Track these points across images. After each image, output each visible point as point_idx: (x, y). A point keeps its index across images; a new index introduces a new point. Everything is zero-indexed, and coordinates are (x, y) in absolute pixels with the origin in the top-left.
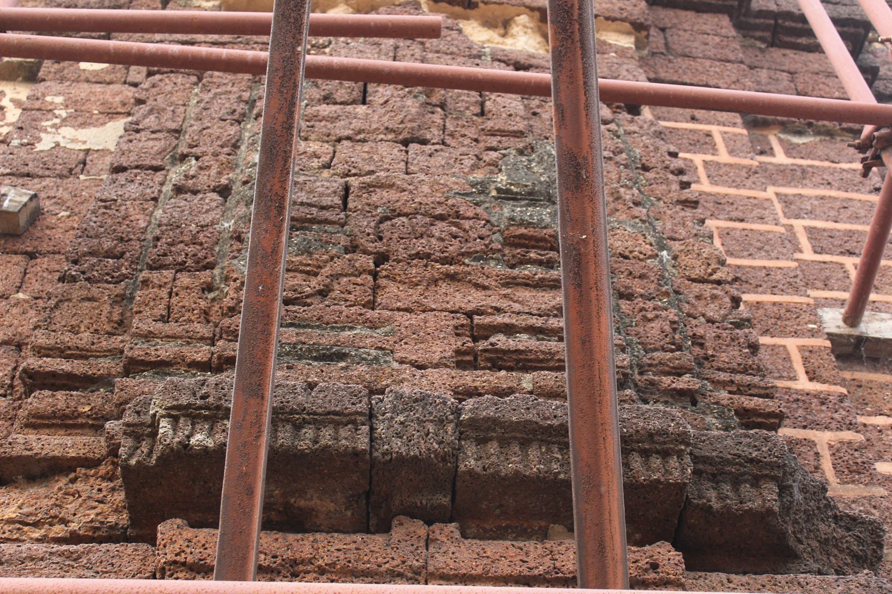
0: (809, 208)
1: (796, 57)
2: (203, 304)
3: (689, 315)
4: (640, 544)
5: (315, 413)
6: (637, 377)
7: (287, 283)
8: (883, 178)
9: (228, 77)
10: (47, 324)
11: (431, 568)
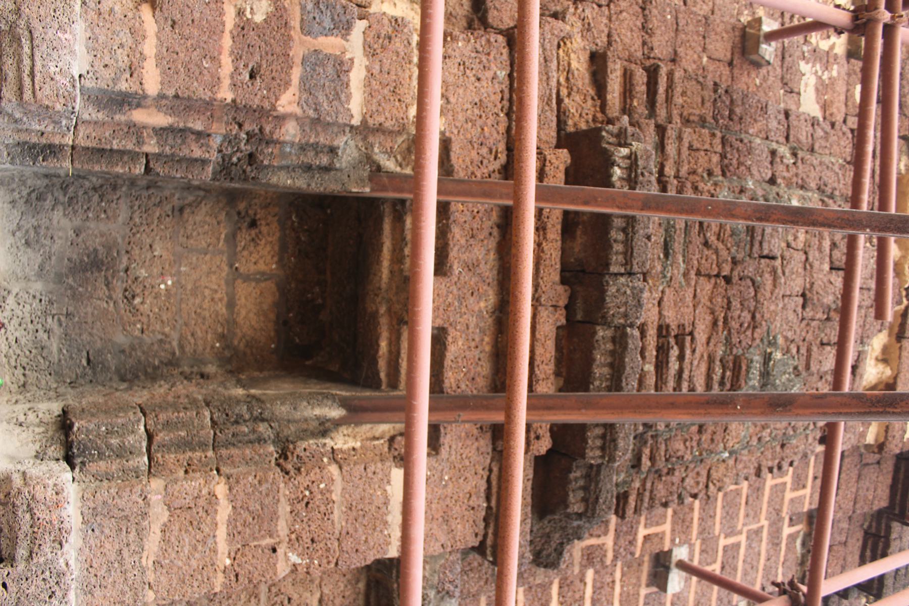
0: (753, 545)
1: (856, 548)
2: (700, 170)
3: (687, 467)
4: (551, 430)
5: (632, 240)
6: (650, 434)
7: (714, 223)
8: (770, 594)
9: (849, 181)
10: (687, 77)
11: (540, 308)
